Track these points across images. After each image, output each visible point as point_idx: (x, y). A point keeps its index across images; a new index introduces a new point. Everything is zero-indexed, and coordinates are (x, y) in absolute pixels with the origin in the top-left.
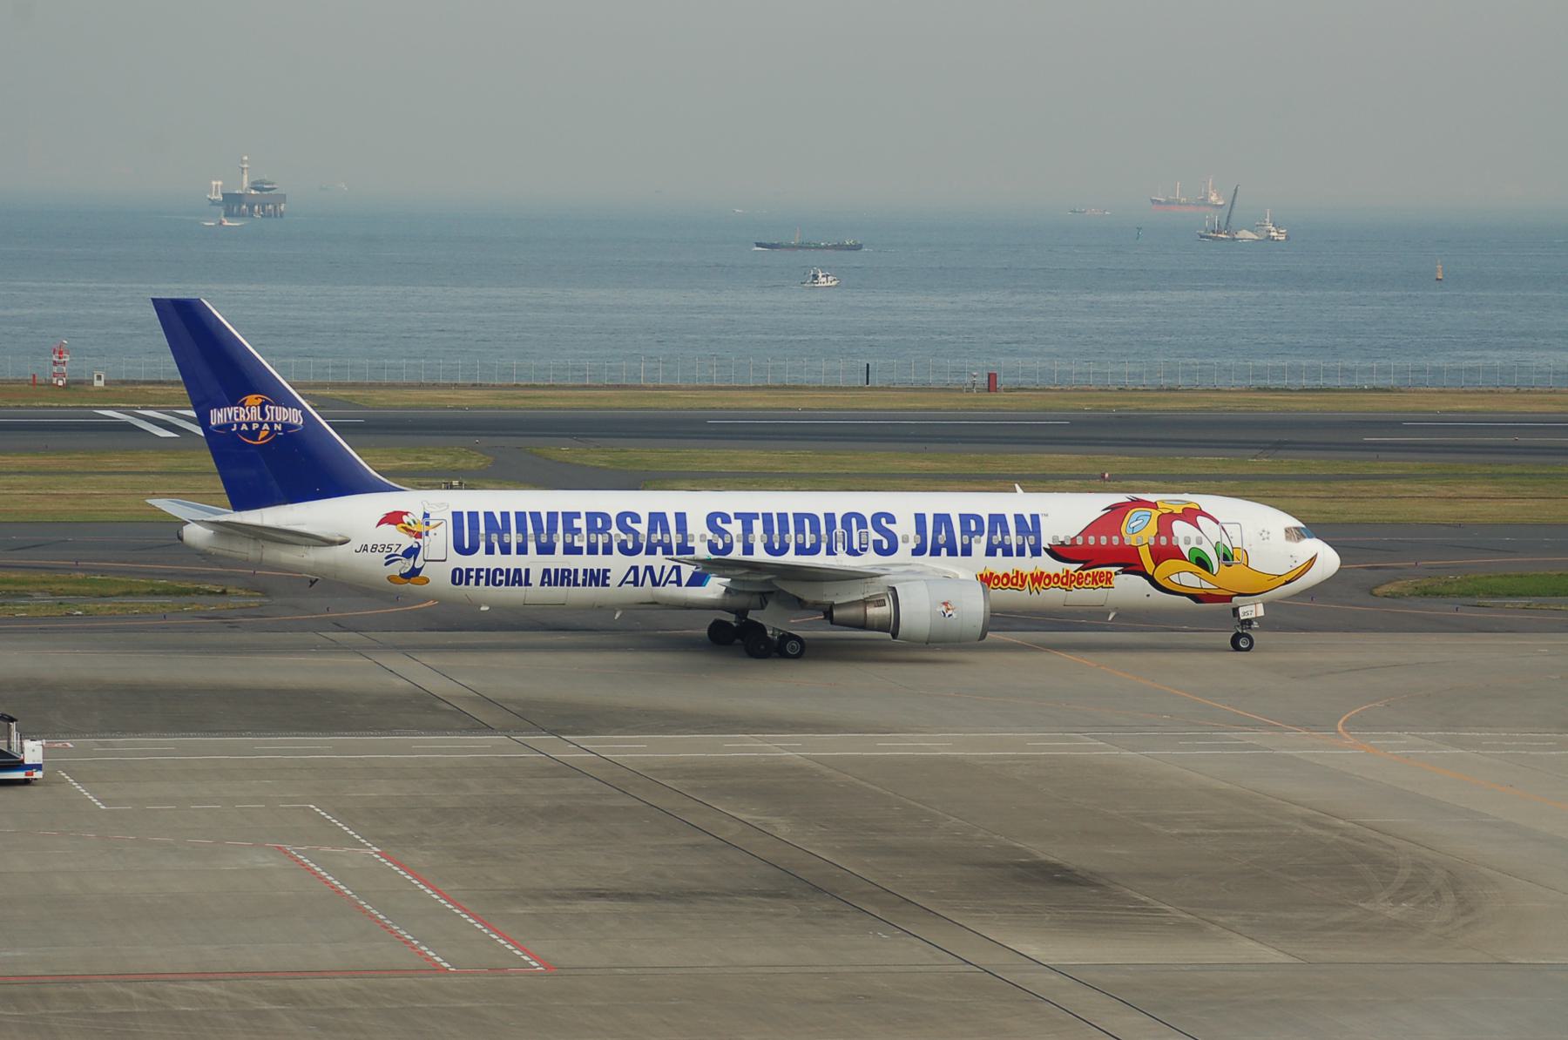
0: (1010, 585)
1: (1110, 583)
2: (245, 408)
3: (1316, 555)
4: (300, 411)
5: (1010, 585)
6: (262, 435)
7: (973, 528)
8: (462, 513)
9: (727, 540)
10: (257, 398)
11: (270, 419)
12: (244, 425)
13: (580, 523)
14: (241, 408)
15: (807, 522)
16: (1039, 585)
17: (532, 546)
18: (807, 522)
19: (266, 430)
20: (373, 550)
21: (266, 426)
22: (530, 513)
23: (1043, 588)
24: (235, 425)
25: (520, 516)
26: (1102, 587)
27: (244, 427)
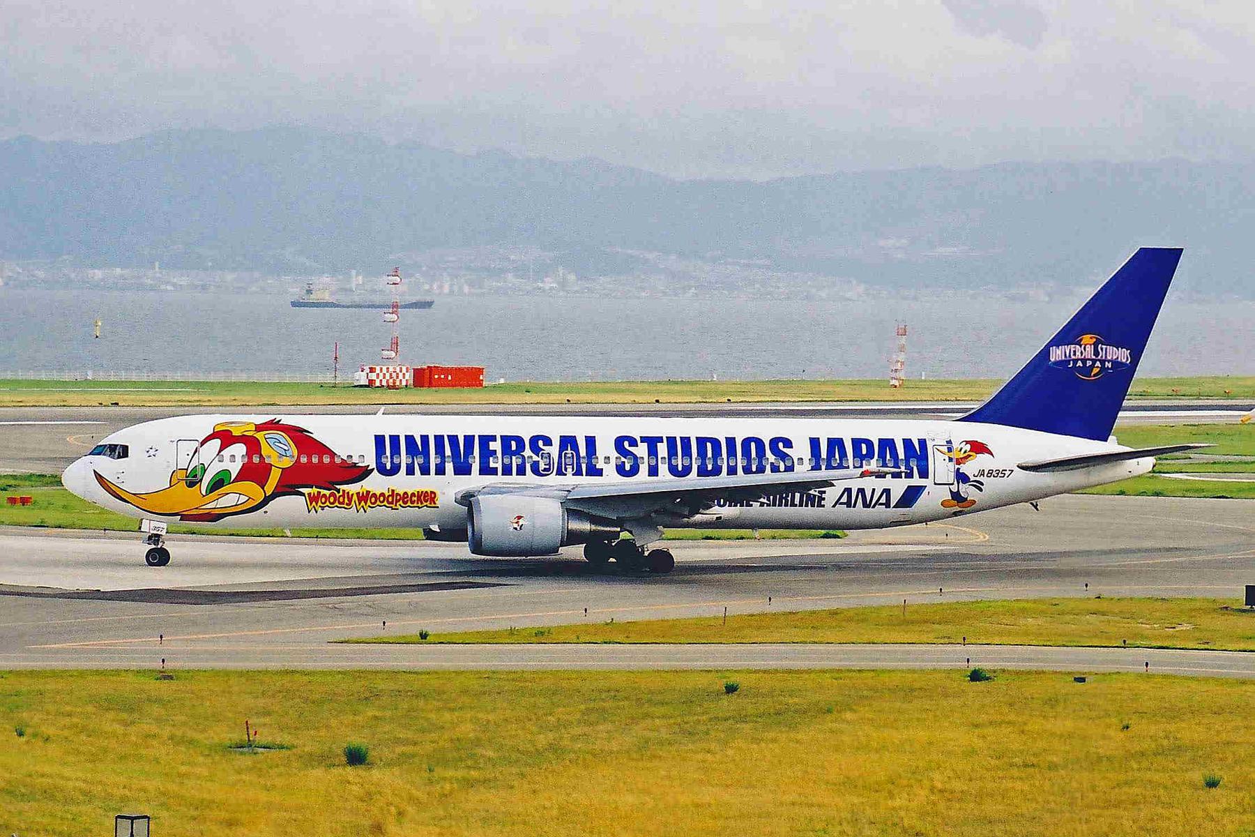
0: (337, 504)
1: (435, 503)
2: (1081, 346)
3: (94, 471)
4: (1129, 351)
5: (337, 504)
6: (1095, 371)
7: (864, 452)
8: (443, 436)
9: (789, 464)
10: (1091, 338)
11: (1102, 357)
12: (1080, 362)
13: (496, 446)
14: (1078, 346)
15: (709, 445)
16: (317, 505)
17: (449, 467)
18: (709, 445)
19: (1098, 367)
20: (989, 475)
21: (1098, 364)
22: (448, 436)
23: (369, 506)
24: (1071, 362)
25: (439, 439)
26: (426, 506)
27: (1080, 364)
